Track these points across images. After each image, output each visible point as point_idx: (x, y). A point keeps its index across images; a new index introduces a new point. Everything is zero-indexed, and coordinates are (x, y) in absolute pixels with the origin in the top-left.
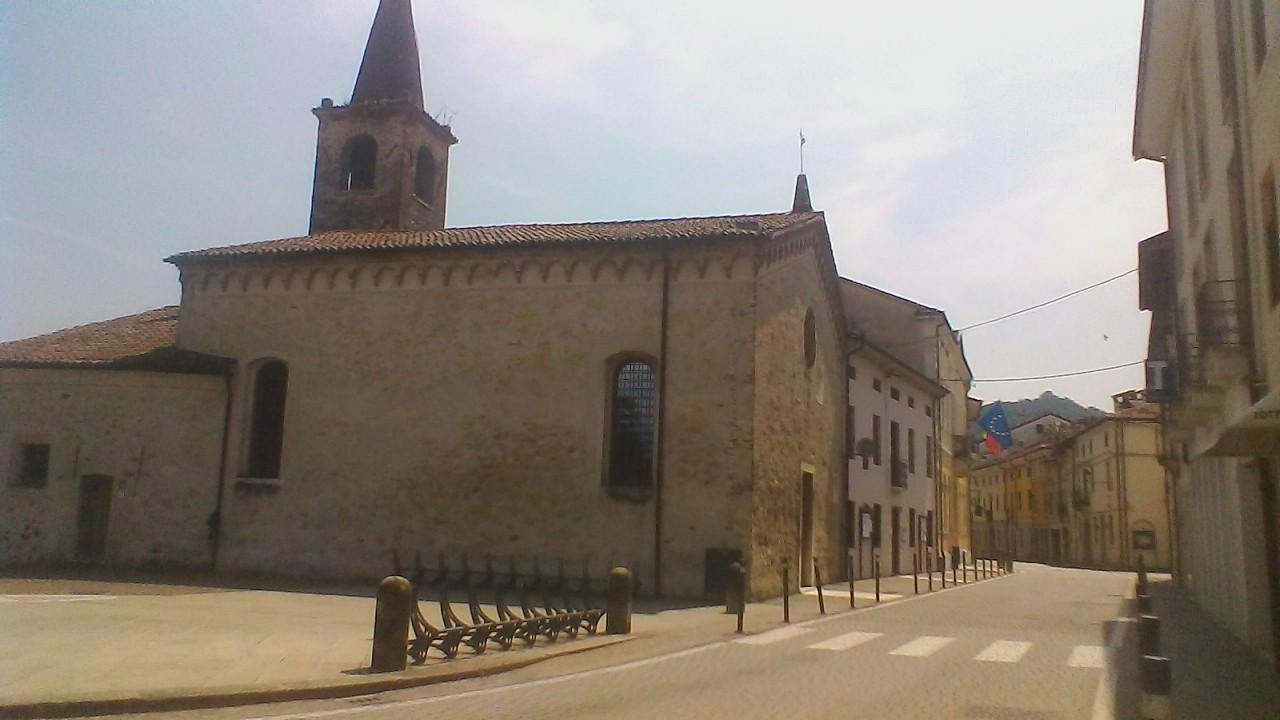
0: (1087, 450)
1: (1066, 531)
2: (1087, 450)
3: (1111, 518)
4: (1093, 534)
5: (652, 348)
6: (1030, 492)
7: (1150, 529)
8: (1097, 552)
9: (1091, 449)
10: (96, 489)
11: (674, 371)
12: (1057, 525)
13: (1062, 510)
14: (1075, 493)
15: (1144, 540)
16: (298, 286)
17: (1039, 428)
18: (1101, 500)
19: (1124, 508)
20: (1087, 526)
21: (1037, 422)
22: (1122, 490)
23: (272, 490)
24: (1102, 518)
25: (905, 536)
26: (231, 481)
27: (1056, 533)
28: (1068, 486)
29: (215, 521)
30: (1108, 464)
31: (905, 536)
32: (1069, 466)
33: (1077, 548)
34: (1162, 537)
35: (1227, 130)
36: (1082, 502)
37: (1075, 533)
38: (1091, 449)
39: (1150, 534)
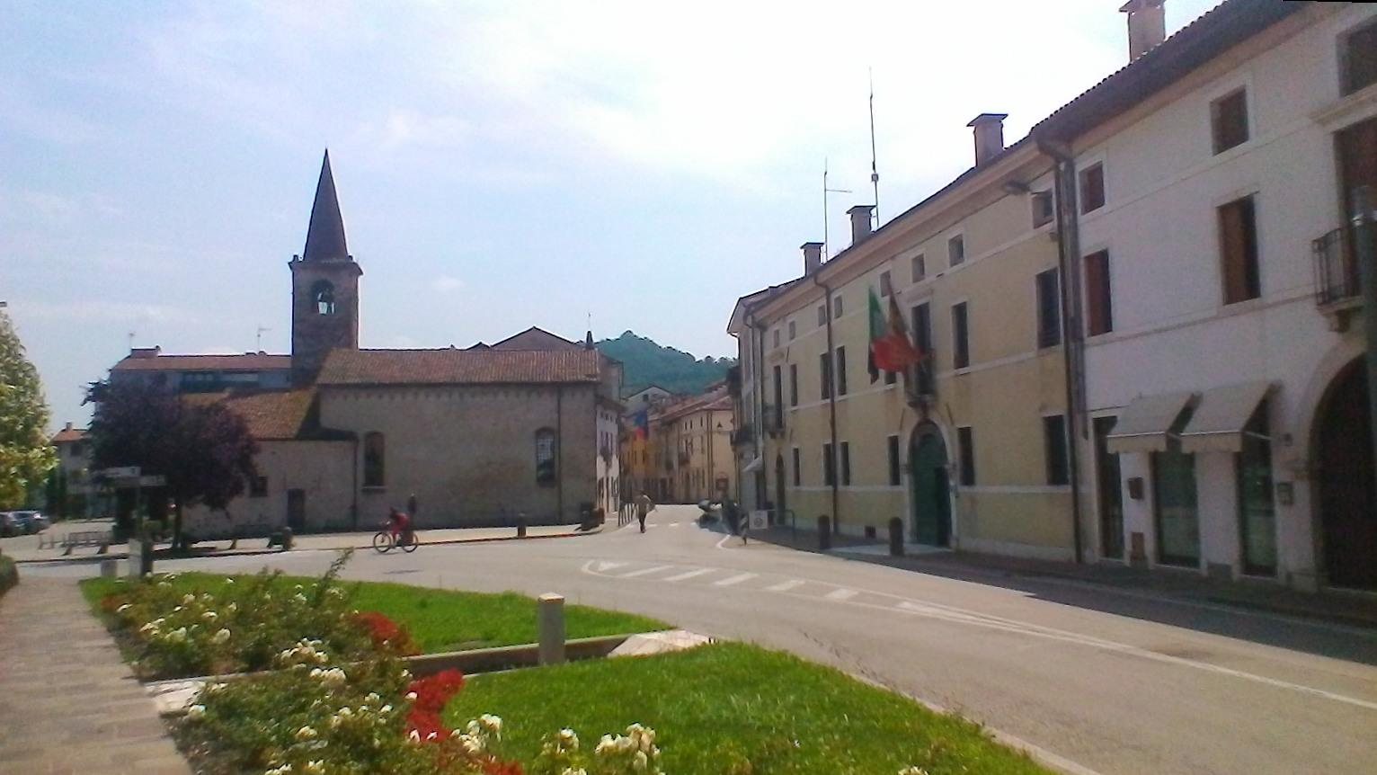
0: (689, 426)
1: (671, 480)
2: (689, 426)
3: (703, 472)
4: (691, 481)
5: (555, 425)
6: (643, 451)
7: (725, 477)
8: (693, 493)
9: (691, 427)
10: (296, 497)
11: (563, 434)
12: (663, 475)
13: (669, 466)
14: (680, 455)
15: (722, 485)
16: (386, 398)
17: (646, 397)
18: (697, 461)
19: (711, 465)
20: (688, 477)
21: (644, 393)
22: (710, 456)
23: (382, 491)
24: (698, 472)
25: (610, 494)
26: (360, 486)
27: (663, 481)
28: (674, 448)
29: (354, 507)
30: (702, 438)
31: (610, 494)
32: (674, 435)
33: (679, 491)
34: (732, 484)
35: (766, 374)
36: (684, 461)
37: (678, 480)
38: (691, 427)
39: (726, 481)
